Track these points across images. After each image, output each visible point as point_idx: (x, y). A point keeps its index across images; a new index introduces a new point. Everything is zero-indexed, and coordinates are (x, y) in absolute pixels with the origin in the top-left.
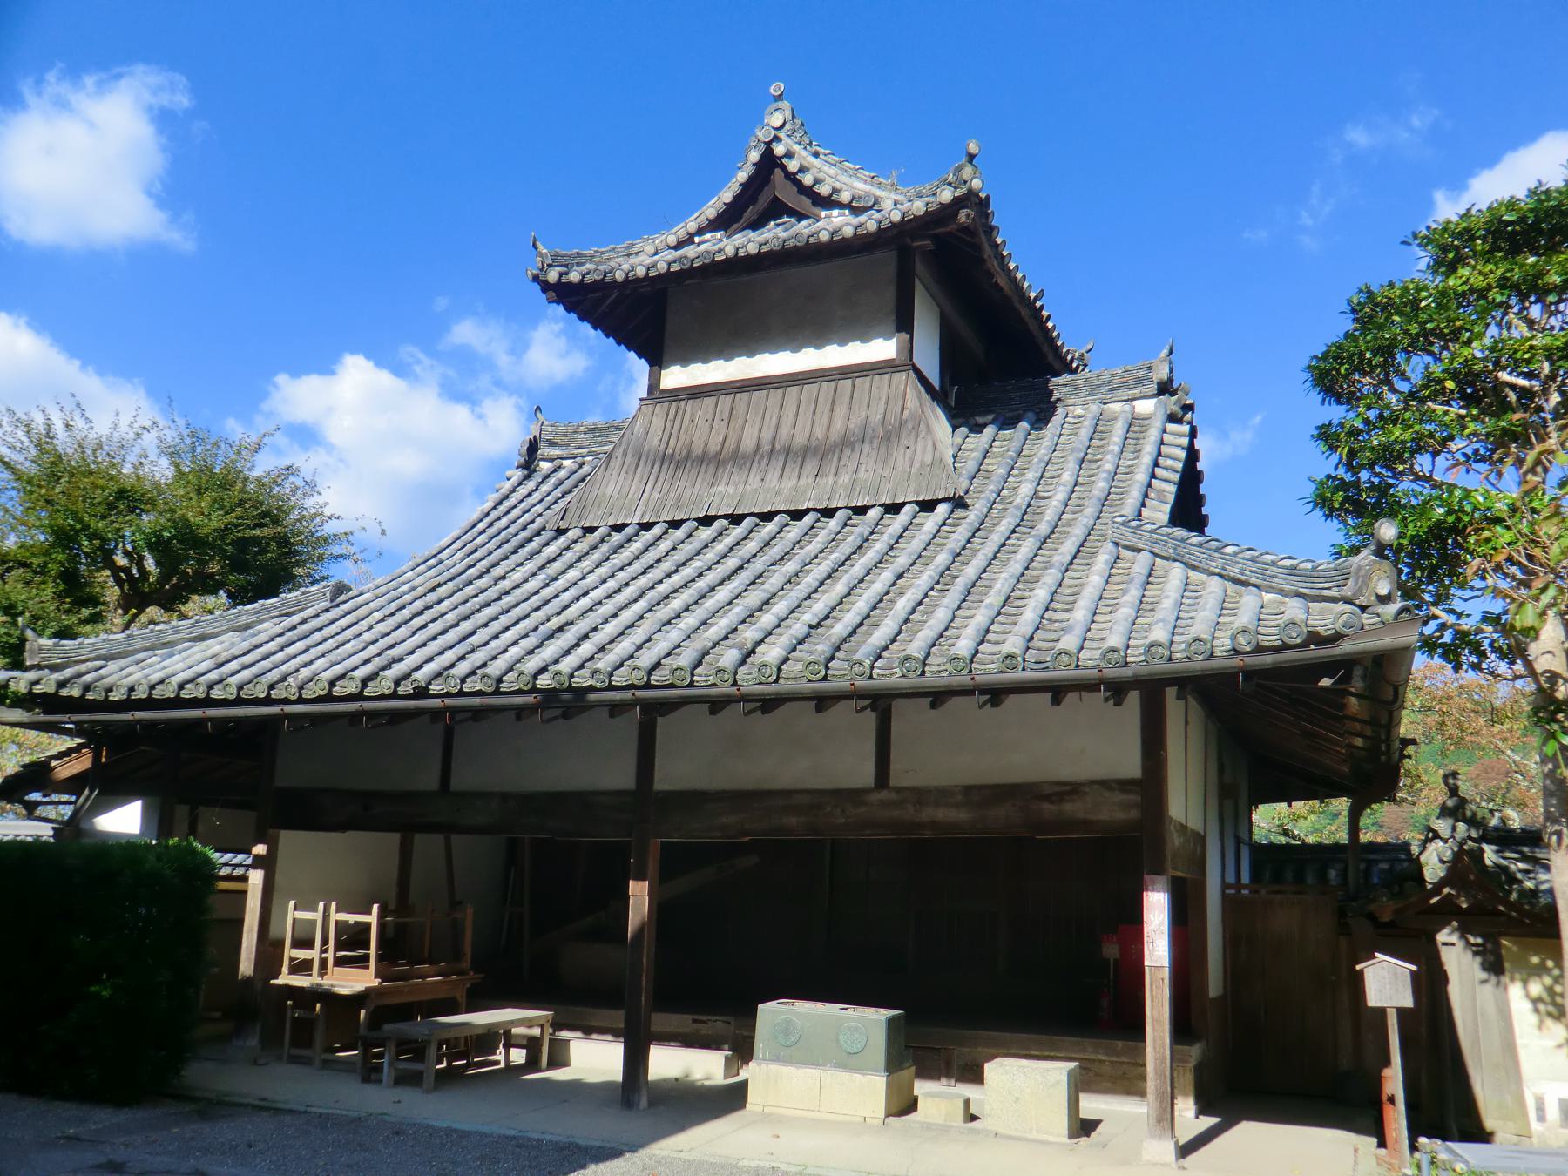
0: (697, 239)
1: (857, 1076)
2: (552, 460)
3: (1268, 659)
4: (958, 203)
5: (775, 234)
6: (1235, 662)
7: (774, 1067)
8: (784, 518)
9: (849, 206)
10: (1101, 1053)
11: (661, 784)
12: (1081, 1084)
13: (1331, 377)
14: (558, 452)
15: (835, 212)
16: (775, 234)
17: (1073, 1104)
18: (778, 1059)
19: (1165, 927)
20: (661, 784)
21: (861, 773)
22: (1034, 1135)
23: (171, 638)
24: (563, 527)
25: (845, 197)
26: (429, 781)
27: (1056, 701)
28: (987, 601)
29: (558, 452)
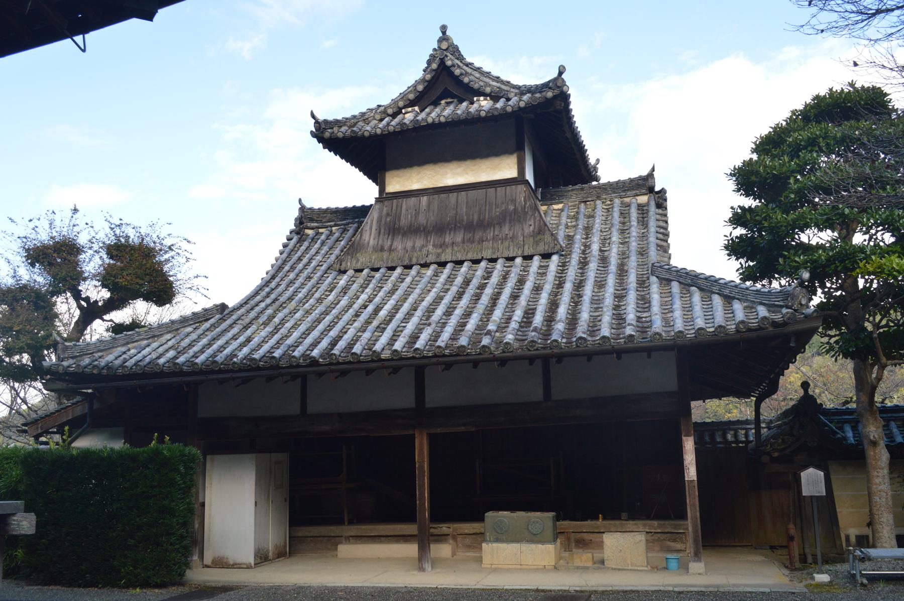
0: (403, 111)
1: (540, 546)
2: (312, 229)
3: (754, 334)
4: (555, 97)
5: (445, 111)
6: (738, 336)
7: (495, 545)
8: (469, 264)
9: (489, 95)
10: (669, 526)
11: (429, 405)
12: (558, 518)
13: (357, 144)
14: (316, 224)
15: (482, 98)
16: (445, 111)
17: (555, 526)
18: (498, 540)
19: (694, 462)
20: (429, 405)
21: (538, 394)
22: (630, 567)
23: (137, 338)
24: (342, 268)
25: (488, 90)
26: (294, 408)
27: (649, 356)
28: (455, 283)
29: (316, 224)
